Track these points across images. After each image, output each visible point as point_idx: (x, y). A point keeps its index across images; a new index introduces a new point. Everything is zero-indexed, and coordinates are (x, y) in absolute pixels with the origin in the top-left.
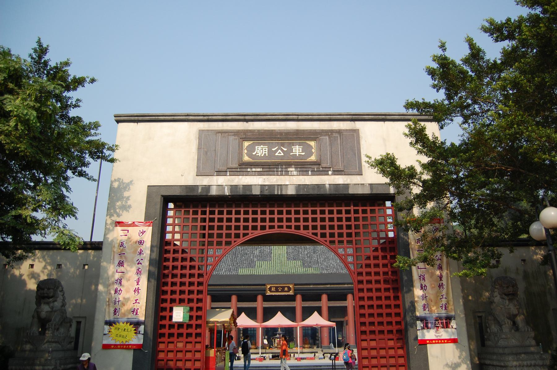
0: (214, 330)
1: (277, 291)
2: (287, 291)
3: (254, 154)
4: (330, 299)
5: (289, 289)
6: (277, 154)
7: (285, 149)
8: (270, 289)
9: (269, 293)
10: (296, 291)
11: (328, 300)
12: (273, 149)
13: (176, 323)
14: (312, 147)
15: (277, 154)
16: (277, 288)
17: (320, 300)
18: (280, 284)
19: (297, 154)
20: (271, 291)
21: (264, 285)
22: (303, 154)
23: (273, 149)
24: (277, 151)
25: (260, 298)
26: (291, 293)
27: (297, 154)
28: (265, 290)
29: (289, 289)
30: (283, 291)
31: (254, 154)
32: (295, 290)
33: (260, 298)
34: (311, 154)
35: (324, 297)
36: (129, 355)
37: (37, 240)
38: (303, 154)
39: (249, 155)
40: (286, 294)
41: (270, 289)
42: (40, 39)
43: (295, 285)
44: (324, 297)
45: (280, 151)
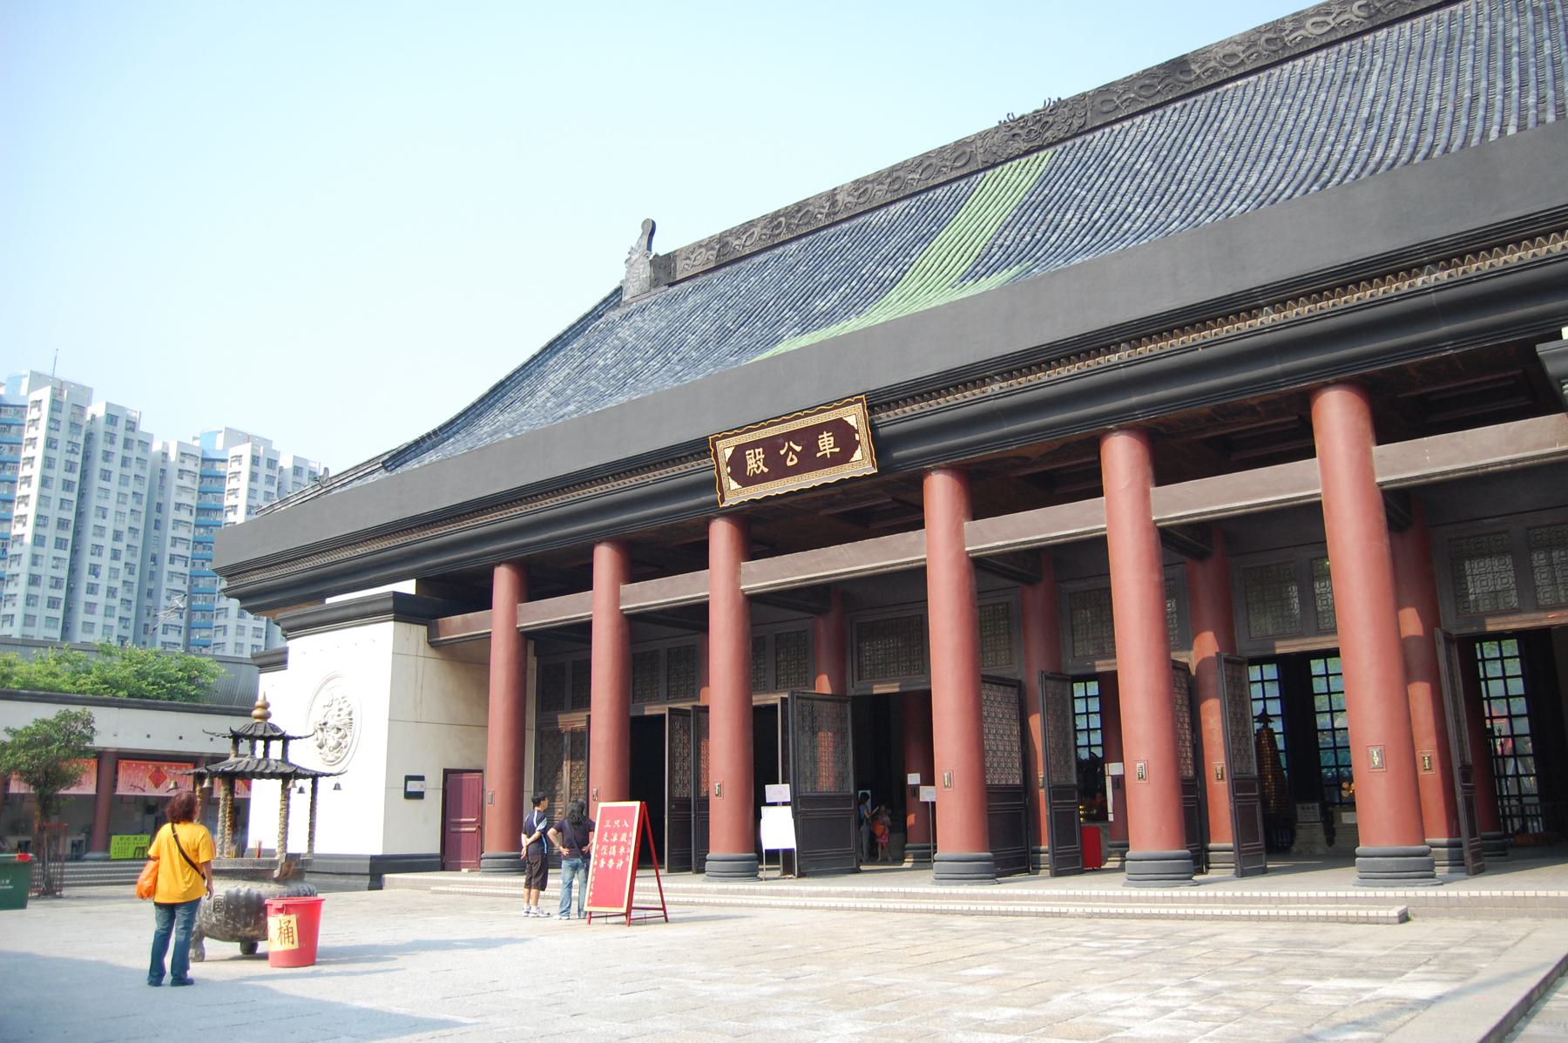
1: (778, 469)
4: (1395, 416)
16: (771, 447)
17: (1085, 481)
20: (746, 480)
21: (701, 448)
24: (787, 454)
26: (861, 463)
28: (711, 485)
29: (843, 433)
30: (811, 461)
32: (882, 446)
35: (1337, 414)
43: (876, 402)
44: (1337, 414)
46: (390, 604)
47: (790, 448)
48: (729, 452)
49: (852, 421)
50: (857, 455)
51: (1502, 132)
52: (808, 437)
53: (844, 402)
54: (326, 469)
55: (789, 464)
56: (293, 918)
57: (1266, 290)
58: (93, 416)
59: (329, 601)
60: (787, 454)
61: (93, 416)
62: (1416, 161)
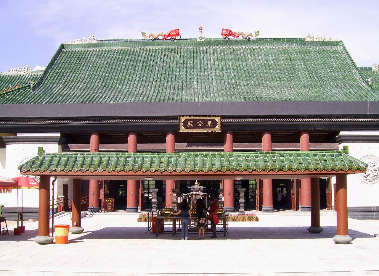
0: (86, 183)
1: (195, 126)
2: (211, 127)
5: (214, 123)
7: (202, 123)
8: (185, 124)
9: (183, 130)
10: (226, 128)
11: (272, 142)
12: (198, 123)
18: (201, 116)
19: (210, 125)
20: (186, 127)
21: (176, 118)
23: (198, 123)
24: (199, 124)
25: (170, 138)
26: (217, 129)
27: (210, 125)
29: (214, 123)
30: (204, 126)
32: (223, 126)
33: (170, 138)
40: (210, 130)
41: (185, 124)
43: (224, 117)
46: (59, 140)
47: (200, 123)
48: (183, 120)
49: (217, 120)
50: (217, 127)
51: (110, 102)
52: (205, 121)
53: (217, 116)
54: (143, 34)
55: (199, 126)
56: (39, 177)
57: (274, 116)
58: (140, 220)
59: (19, 135)
60: (199, 124)
61: (140, 220)
62: (43, 103)
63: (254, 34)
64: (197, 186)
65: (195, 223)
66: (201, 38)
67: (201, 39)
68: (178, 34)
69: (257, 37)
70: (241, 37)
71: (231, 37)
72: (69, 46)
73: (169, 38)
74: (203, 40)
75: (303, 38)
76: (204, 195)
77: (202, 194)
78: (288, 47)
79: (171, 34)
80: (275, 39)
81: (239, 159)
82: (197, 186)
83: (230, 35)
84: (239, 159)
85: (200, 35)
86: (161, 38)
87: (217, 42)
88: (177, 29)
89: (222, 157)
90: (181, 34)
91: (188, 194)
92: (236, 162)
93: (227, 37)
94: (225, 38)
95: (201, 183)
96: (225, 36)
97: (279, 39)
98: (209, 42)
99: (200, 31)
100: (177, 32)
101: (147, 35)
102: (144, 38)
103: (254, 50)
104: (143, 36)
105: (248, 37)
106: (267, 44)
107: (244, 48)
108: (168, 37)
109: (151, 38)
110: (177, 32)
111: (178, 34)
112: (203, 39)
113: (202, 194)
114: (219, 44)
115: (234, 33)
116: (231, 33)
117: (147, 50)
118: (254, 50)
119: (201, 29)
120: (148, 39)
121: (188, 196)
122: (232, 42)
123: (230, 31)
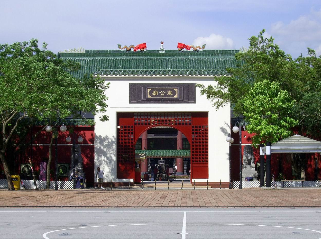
3: (152, 94)
6: (161, 95)
7: (165, 92)
12: (160, 92)
13: (70, 180)
14: (149, 95)
15: (161, 95)
19: (170, 94)
22: (172, 94)
23: (160, 92)
24: (161, 93)
27: (170, 94)
31: (152, 94)
34: (175, 94)
36: (193, 118)
37: (228, 152)
38: (172, 94)
39: (150, 95)
42: (309, 49)
44: (119, 135)
45: (162, 93)
54: (119, 46)
60: (161, 93)
63: (201, 47)
64: (162, 160)
65: (32, 145)
66: (163, 50)
67: (162, 51)
68: (145, 47)
69: (204, 49)
70: (191, 49)
71: (184, 50)
72: (64, 55)
73: (139, 50)
74: (164, 52)
75: (238, 50)
76: (165, 165)
77: (165, 164)
78: (226, 59)
79: (140, 47)
80: (217, 51)
81: (178, 152)
82: (162, 160)
83: (183, 48)
84: (178, 152)
85: (162, 48)
86: (132, 49)
87: (174, 54)
88: (145, 43)
89: (172, 151)
90: (147, 46)
91: (158, 164)
92: (177, 154)
93: (181, 50)
94: (180, 51)
95: (163, 159)
96: (180, 49)
97: (220, 51)
98: (169, 53)
99: (162, 44)
100: (144, 46)
101: (122, 47)
102: (120, 49)
103: (201, 61)
104: (119, 48)
105: (197, 50)
106: (211, 55)
107: (193, 59)
108: (138, 49)
109: (125, 49)
110: (144, 46)
111: (145, 47)
112: (164, 50)
113: (165, 164)
114: (175, 55)
115: (187, 46)
116: (184, 46)
117: (123, 60)
118: (201, 61)
119: (162, 43)
120: (123, 50)
121: (158, 165)
122: (185, 54)
123: (184, 45)
